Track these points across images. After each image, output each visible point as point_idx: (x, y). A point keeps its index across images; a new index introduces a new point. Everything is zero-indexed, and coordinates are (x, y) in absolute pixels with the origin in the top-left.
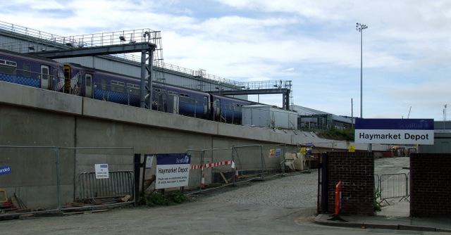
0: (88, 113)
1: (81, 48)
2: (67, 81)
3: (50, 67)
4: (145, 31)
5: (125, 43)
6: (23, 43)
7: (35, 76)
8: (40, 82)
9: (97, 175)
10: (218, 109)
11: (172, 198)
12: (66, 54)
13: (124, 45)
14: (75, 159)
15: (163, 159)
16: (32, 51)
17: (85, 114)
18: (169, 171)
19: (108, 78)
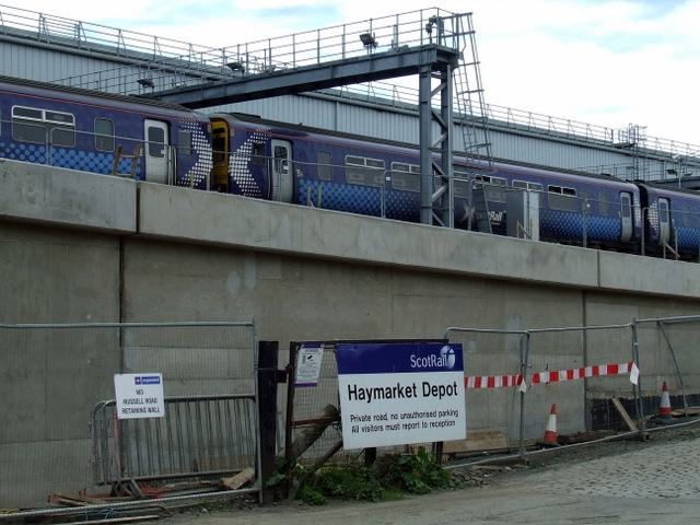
0: (154, 225)
1: (269, 74)
2: (220, 159)
3: (669, 200)
4: (433, 13)
6: (125, 71)
7: (131, 147)
8: (143, 166)
9: (120, 406)
10: (665, 226)
11: (396, 474)
12: (231, 91)
13: (374, 58)
16: (148, 90)
17: (144, 229)
18: (389, 393)
19: (341, 148)
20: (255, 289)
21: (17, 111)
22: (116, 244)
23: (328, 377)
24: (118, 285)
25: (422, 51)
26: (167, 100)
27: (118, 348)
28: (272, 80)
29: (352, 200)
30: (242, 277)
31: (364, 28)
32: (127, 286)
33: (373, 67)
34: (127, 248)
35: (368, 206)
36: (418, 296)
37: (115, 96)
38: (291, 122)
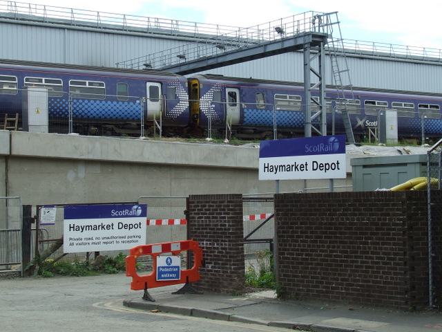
4: (315, 14)
5: (284, 36)
13: (283, 40)
14: (7, 215)
15: (73, 211)
16: (183, 61)
17: (14, 153)
20: (84, 178)
21: (72, 83)
22: (4, 160)
23: (59, 221)
24: (5, 178)
25: (305, 36)
26: (172, 71)
27: (5, 208)
28: (241, 53)
29: (288, 119)
30: (77, 173)
31: (278, 24)
32: (9, 179)
33: (283, 45)
34: (9, 161)
35: (290, 122)
36: (188, 178)
37: (137, 71)
38: (245, 77)
